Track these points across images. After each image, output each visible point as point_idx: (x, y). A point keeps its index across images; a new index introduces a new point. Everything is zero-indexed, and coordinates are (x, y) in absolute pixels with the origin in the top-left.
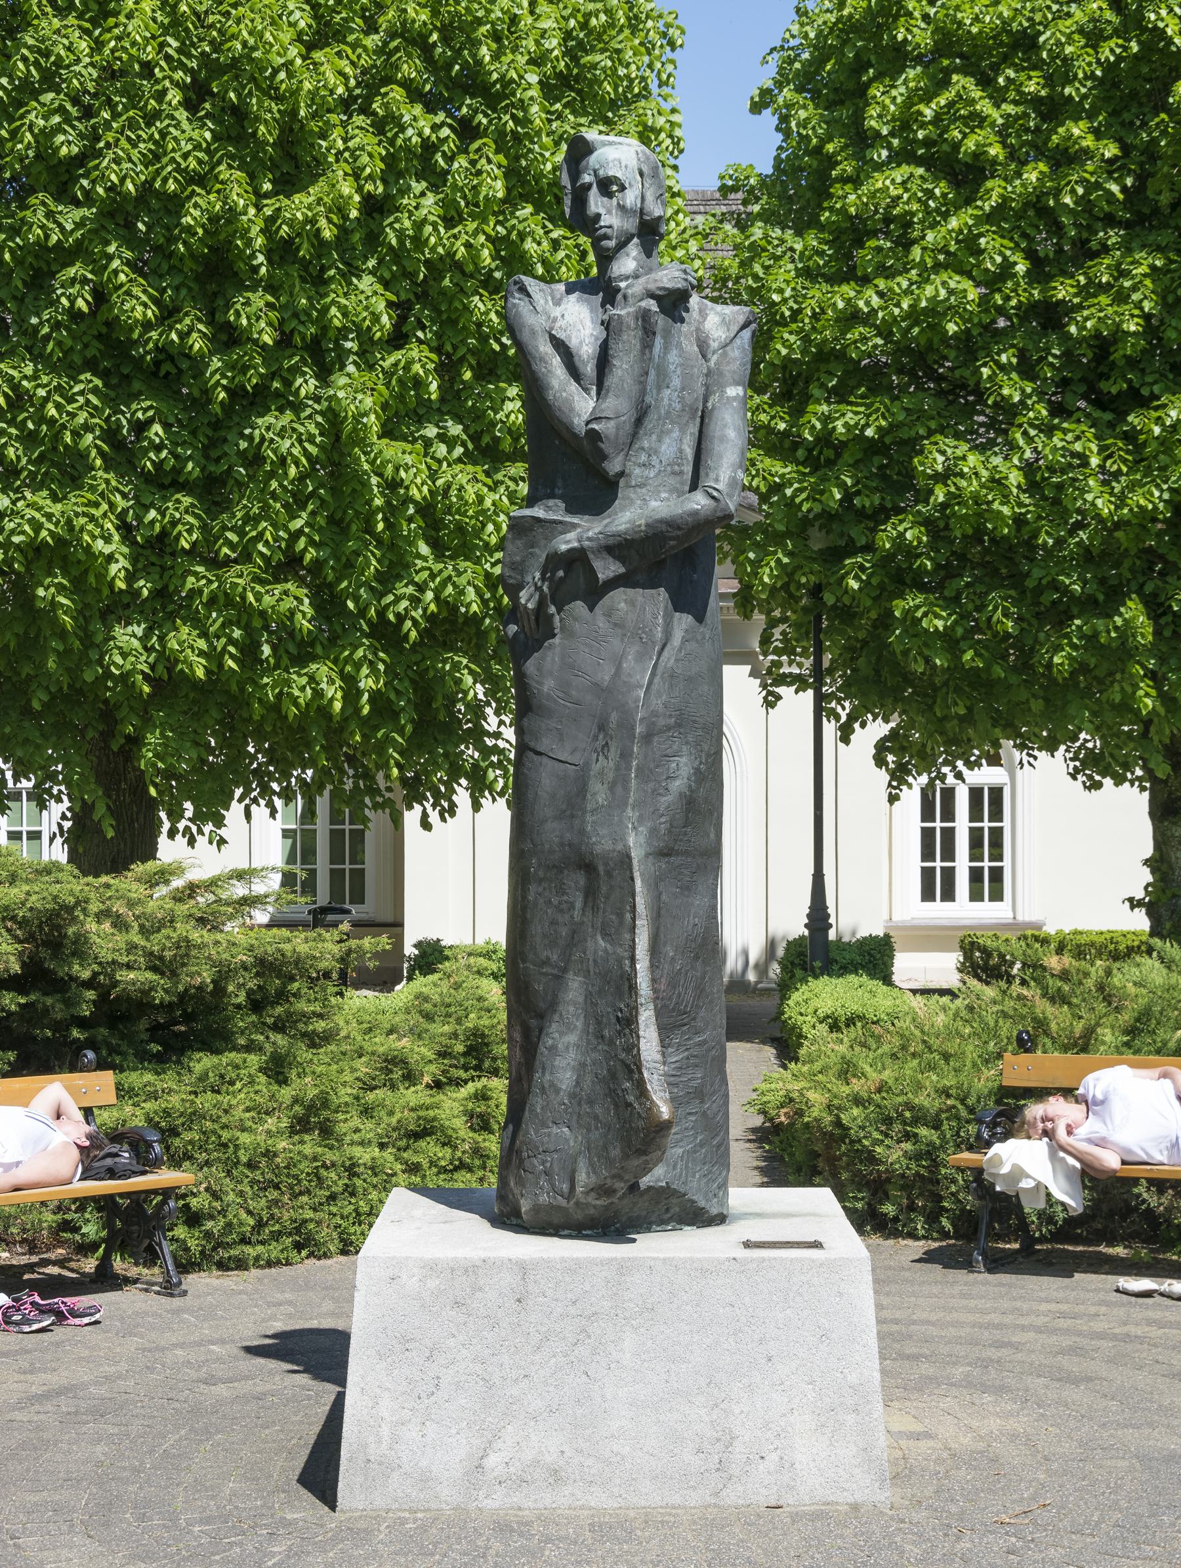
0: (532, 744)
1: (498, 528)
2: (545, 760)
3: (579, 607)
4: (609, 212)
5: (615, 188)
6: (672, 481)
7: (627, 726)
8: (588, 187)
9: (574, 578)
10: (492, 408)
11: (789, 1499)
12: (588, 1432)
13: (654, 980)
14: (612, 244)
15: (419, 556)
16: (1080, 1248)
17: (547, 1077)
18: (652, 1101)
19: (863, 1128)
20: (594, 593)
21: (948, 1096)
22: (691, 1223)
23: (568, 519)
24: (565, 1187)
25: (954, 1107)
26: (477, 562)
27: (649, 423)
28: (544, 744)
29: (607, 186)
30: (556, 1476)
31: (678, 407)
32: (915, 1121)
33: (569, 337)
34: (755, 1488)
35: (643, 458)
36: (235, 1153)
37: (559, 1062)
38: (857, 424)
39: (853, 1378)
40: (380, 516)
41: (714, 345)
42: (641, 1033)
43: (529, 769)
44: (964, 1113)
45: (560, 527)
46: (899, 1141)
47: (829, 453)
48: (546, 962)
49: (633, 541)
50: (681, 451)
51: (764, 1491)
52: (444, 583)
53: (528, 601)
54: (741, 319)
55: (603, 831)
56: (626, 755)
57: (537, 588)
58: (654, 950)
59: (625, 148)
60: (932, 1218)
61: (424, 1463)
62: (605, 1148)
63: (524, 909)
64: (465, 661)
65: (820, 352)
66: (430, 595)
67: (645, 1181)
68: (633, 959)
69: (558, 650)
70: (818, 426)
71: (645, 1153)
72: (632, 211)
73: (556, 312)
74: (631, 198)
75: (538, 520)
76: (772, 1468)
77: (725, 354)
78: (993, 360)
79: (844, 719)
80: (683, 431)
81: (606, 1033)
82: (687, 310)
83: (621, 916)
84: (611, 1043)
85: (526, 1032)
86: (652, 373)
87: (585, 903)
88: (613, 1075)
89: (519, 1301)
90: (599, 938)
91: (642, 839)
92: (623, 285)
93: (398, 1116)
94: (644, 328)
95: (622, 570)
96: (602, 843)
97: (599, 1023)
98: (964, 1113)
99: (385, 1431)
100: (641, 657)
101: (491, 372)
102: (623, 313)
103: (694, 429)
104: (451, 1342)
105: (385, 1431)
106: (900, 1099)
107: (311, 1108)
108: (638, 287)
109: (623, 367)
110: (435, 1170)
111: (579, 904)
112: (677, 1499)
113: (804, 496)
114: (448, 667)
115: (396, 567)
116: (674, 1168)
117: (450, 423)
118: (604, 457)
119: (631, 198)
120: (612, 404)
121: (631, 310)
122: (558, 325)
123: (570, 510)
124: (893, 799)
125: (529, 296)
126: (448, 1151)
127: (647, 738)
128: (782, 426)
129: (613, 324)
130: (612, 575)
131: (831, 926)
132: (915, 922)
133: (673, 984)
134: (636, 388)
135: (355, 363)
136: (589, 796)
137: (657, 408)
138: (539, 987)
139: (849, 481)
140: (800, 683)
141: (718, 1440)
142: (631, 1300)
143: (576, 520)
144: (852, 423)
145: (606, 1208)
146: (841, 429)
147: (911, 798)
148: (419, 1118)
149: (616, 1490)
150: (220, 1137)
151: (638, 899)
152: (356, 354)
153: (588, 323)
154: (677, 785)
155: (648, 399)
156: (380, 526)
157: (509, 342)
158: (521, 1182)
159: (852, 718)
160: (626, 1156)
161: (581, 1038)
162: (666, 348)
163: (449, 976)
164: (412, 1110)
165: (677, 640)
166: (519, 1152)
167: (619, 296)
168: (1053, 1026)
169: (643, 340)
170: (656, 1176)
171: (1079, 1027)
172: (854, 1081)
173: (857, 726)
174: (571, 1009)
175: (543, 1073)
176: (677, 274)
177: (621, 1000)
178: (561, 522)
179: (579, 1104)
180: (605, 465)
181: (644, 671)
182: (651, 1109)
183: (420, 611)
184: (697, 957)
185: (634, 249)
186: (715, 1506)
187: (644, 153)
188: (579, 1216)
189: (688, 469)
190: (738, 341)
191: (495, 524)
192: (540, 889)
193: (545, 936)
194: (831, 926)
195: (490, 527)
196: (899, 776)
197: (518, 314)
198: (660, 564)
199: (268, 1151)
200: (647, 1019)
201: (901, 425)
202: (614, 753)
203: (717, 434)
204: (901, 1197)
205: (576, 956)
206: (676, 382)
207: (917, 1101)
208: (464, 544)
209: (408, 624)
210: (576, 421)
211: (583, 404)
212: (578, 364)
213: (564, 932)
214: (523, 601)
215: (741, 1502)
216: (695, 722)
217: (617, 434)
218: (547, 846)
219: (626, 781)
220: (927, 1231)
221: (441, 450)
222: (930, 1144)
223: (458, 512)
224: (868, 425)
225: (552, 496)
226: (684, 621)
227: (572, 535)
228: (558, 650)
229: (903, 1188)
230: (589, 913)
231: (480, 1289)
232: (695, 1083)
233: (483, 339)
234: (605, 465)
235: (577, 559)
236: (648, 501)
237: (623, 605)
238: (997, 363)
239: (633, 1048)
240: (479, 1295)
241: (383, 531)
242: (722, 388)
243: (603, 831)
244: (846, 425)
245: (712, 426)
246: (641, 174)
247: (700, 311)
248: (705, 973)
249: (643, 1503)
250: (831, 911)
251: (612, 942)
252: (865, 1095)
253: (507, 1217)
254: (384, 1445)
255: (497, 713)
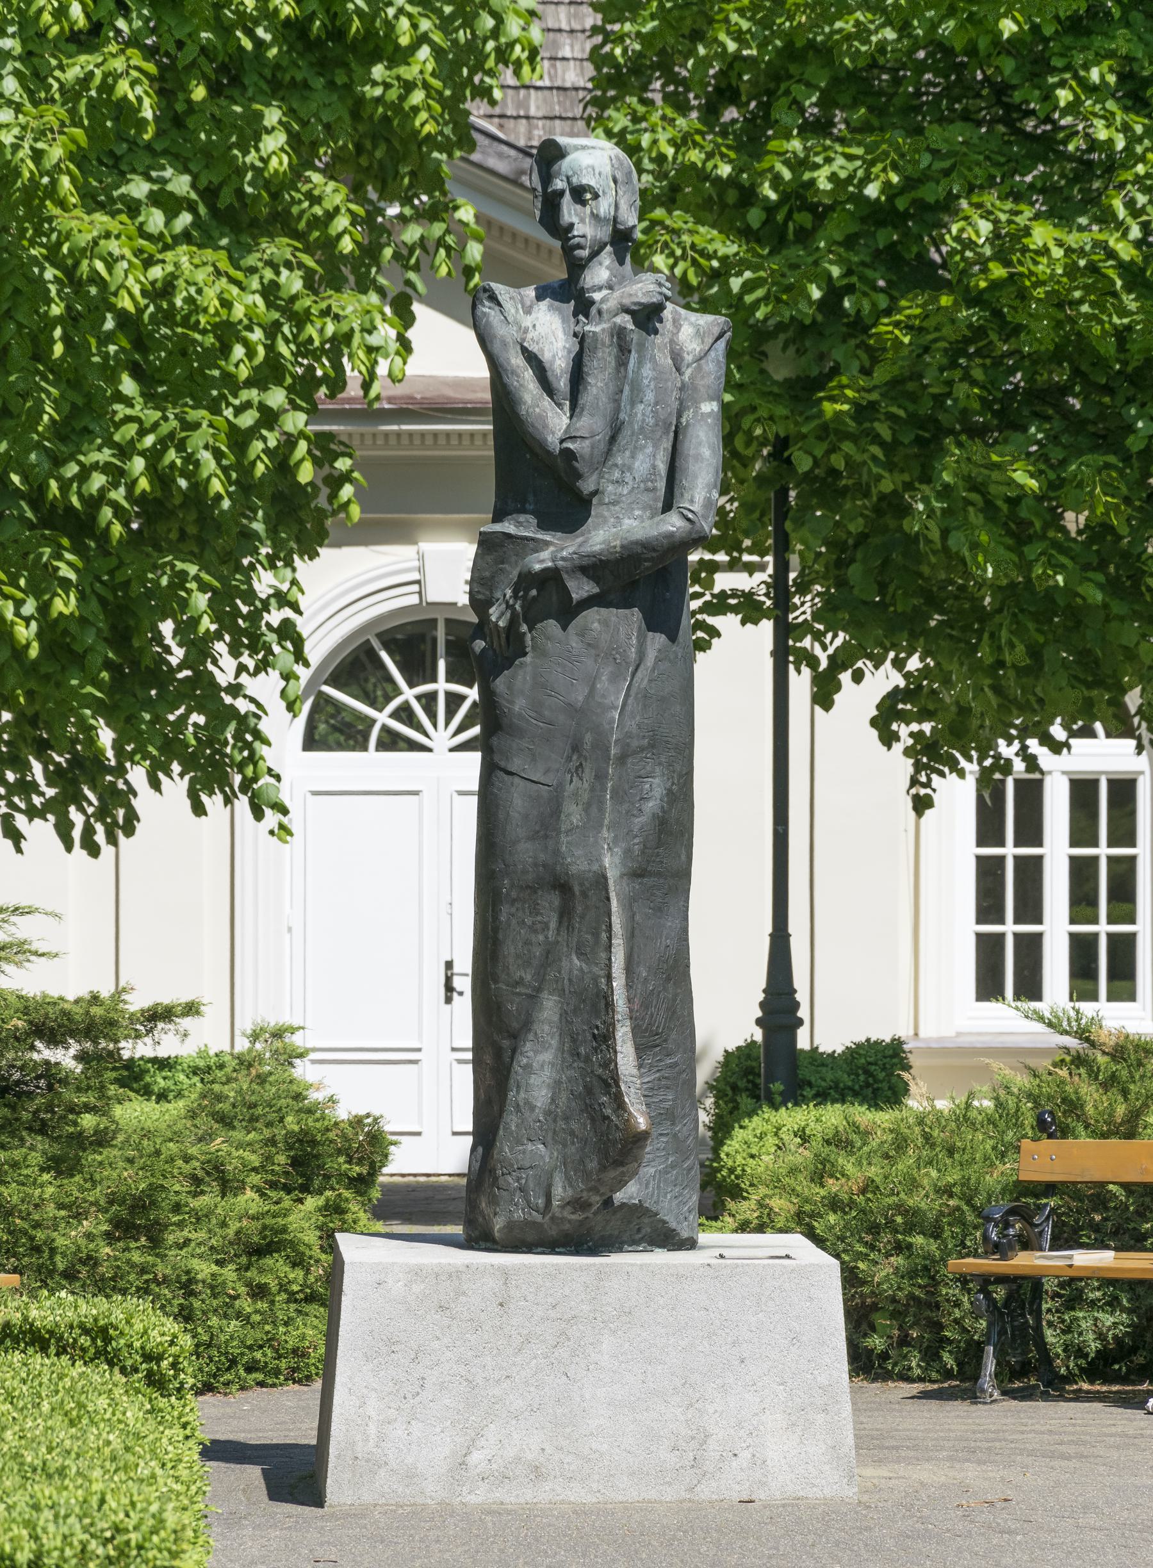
0: (502, 764)
1: (251, 354)
2: (517, 780)
3: (551, 626)
4: (582, 221)
5: (588, 196)
6: (646, 498)
7: (601, 746)
8: (561, 193)
9: (547, 598)
10: (237, 145)
11: (761, 1495)
12: (568, 1430)
13: (629, 1000)
14: (585, 253)
15: (120, 398)
16: (1115, 1388)
17: (522, 1095)
18: (630, 1113)
19: (842, 1239)
20: (567, 612)
21: (951, 1196)
22: (662, 1245)
23: (539, 536)
24: (541, 1202)
25: (958, 1208)
26: (215, 410)
27: (622, 440)
28: (515, 765)
29: (579, 193)
30: (537, 1473)
31: (651, 421)
32: (910, 1228)
33: (542, 350)
34: (728, 1484)
35: (617, 475)
36: (51, 1258)
37: (533, 1080)
38: (851, 177)
39: (823, 1380)
40: (58, 332)
41: (689, 358)
42: (618, 1048)
43: (500, 789)
44: (970, 1217)
45: (531, 544)
46: (888, 1255)
47: (804, 219)
48: (520, 982)
49: (608, 561)
50: (654, 467)
51: (737, 1487)
52: (163, 444)
53: (499, 618)
54: (716, 331)
55: (578, 852)
56: (601, 777)
57: (508, 606)
58: (629, 969)
59: (598, 153)
60: (931, 1355)
61: (410, 1460)
62: (582, 1161)
63: (496, 930)
64: (193, 569)
65: (789, 44)
66: (138, 464)
67: (619, 1197)
68: (609, 978)
69: (529, 669)
70: (787, 175)
71: (622, 1164)
72: (606, 220)
73: (527, 321)
74: (604, 207)
75: (509, 536)
76: (745, 1465)
77: (699, 368)
78: (1075, 76)
79: (824, 664)
80: (656, 446)
81: (582, 1050)
82: (661, 321)
83: (596, 935)
84: (587, 1059)
85: (498, 1053)
86: (627, 388)
87: (560, 922)
88: (589, 1091)
89: (501, 1305)
90: (574, 958)
91: (617, 860)
92: (597, 296)
93: (234, 1226)
94: (620, 346)
95: (596, 590)
96: (577, 864)
97: (574, 1040)
98: (970, 1217)
99: (372, 1430)
100: (615, 678)
101: (236, 81)
102: (597, 329)
103: (667, 444)
104: (436, 1344)
105: (372, 1430)
106: (890, 1200)
107: (142, 1204)
108: (611, 304)
109: (598, 384)
110: (285, 1296)
111: (553, 925)
112: (652, 1495)
113: (760, 293)
114: (164, 581)
115: (84, 418)
116: (647, 1187)
117: (168, 173)
118: (579, 476)
119: (604, 207)
120: (585, 423)
121: (605, 326)
122: (529, 336)
123: (543, 526)
124: (921, 805)
125: (499, 305)
126: (298, 1274)
127: (622, 759)
128: (725, 170)
129: (588, 340)
130: (585, 595)
131: (800, 1022)
132: (965, 1041)
133: (645, 1005)
134: (610, 407)
135: (16, 73)
136: (563, 817)
137: (631, 423)
138: (512, 1007)
139: (836, 271)
140: (749, 609)
141: (693, 1438)
142: (608, 1304)
143: (548, 538)
144: (843, 174)
145: (581, 1223)
146: (824, 185)
147: (957, 794)
148: (265, 1227)
149: (595, 1486)
150: (32, 1238)
151: (613, 918)
152: (19, 58)
153: (560, 334)
154: (651, 806)
155: (622, 416)
156: (58, 349)
157: (268, 37)
158: (494, 1201)
159: (839, 662)
160: (603, 1168)
161: (556, 1057)
162: (640, 363)
163: (250, 1066)
164: (253, 1218)
165: (651, 656)
166: (492, 1171)
167: (593, 310)
168: (1089, 1109)
169: (618, 358)
170: (629, 1193)
171: (1121, 1110)
172: (831, 1181)
173: (845, 677)
174: (546, 1028)
175: (518, 1092)
176: (652, 287)
177: (598, 1017)
178: (533, 539)
179: (555, 1121)
180: (579, 484)
181: (618, 692)
182: (628, 1121)
183: (122, 490)
184: (668, 979)
185: (607, 258)
186: (690, 1500)
187: (617, 157)
188: (553, 1232)
189: (661, 485)
190: (712, 354)
191: (246, 343)
192: (513, 910)
193: (518, 956)
194: (800, 1022)
195: (239, 351)
196: (930, 757)
197: (488, 323)
198: (634, 584)
199: (89, 1257)
200: (623, 1034)
201: (924, 178)
202: (588, 774)
203: (692, 452)
204: (891, 1326)
205: (552, 974)
206: (650, 396)
207: (911, 1203)
208: (191, 376)
209: (107, 512)
210: (550, 439)
211: (557, 421)
212: (551, 378)
213: (538, 952)
214: (494, 619)
215: (714, 1497)
216: (667, 742)
217: (592, 454)
218: (520, 867)
219: (601, 802)
220: (924, 1370)
221: (155, 220)
222: (928, 1256)
223: (185, 323)
224: (867, 180)
225: (524, 511)
226: (657, 641)
227: (545, 554)
228: (529, 669)
229: (894, 1315)
230: (564, 933)
231: (464, 1293)
232: (667, 1105)
233: (225, 30)
234: (579, 484)
235: (551, 578)
236: (621, 522)
237: (596, 625)
238: (1083, 83)
239: (610, 1064)
240: (463, 1299)
241: (63, 357)
242: (697, 403)
243: (578, 852)
244: (833, 178)
245: (686, 444)
246: (615, 181)
247: (674, 321)
248: (676, 995)
249: (621, 1498)
250: (802, 996)
251: (587, 961)
252: (845, 1197)
253: (471, 1243)
254: (371, 1443)
255: (235, 652)
